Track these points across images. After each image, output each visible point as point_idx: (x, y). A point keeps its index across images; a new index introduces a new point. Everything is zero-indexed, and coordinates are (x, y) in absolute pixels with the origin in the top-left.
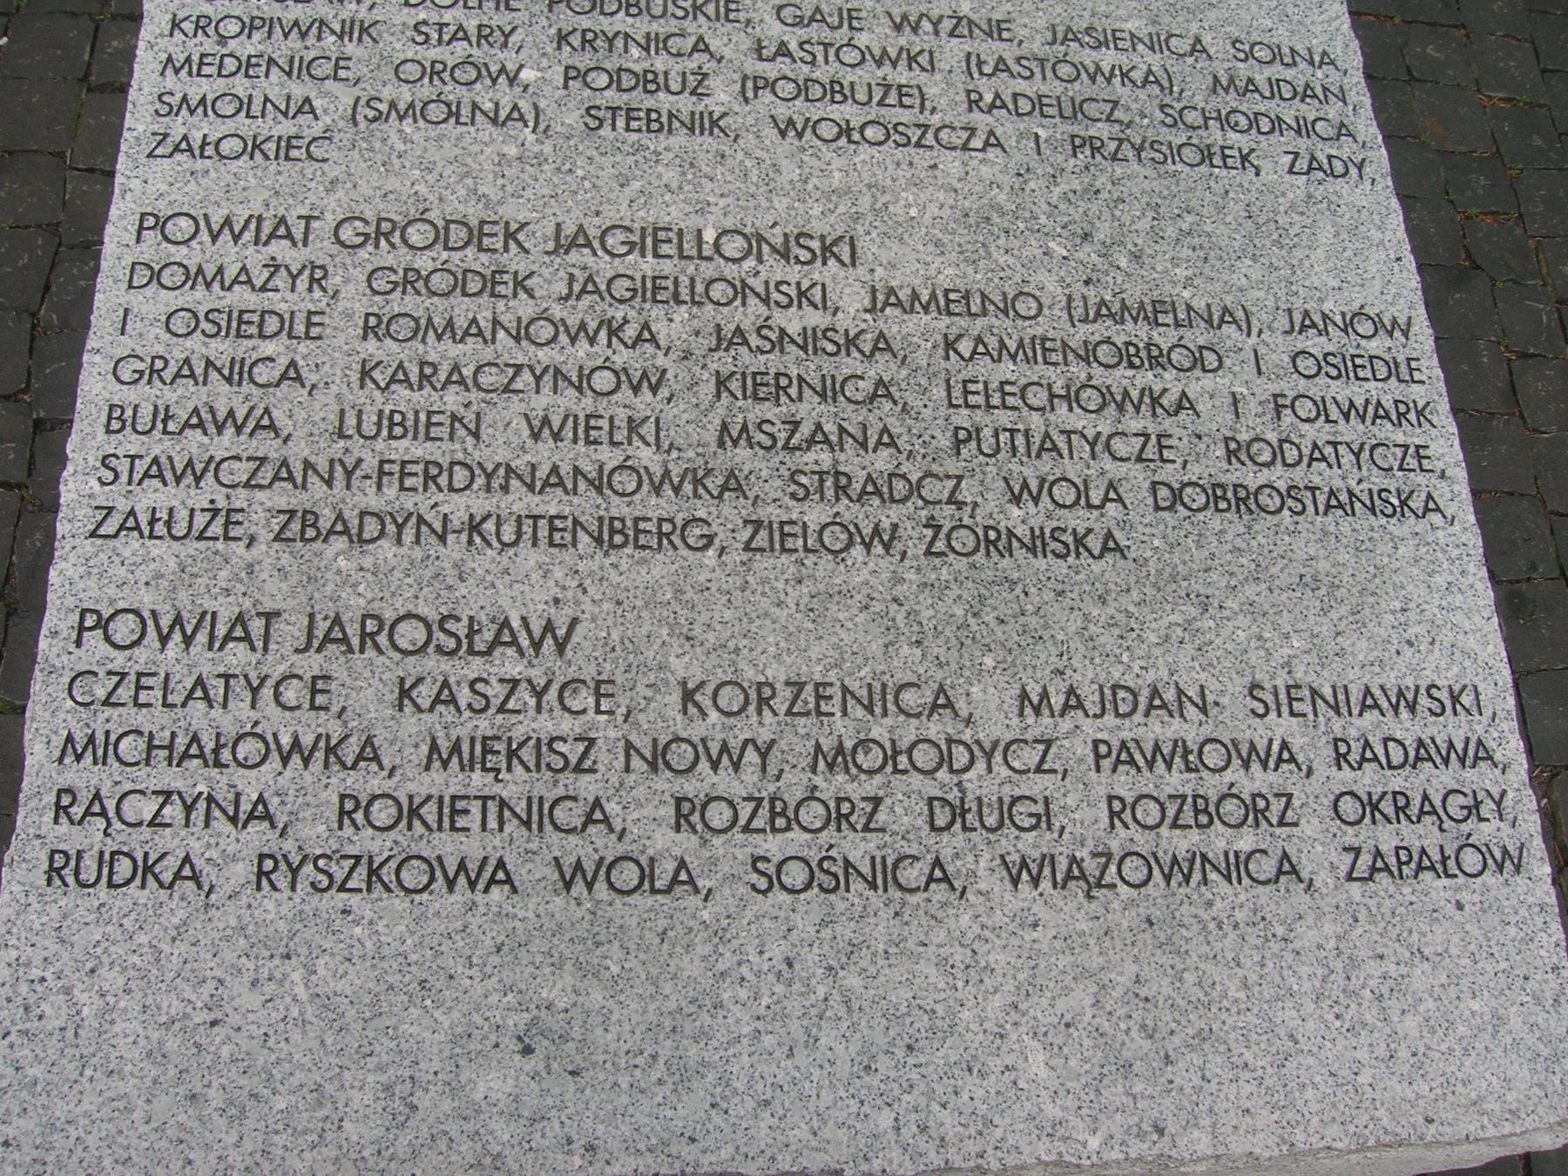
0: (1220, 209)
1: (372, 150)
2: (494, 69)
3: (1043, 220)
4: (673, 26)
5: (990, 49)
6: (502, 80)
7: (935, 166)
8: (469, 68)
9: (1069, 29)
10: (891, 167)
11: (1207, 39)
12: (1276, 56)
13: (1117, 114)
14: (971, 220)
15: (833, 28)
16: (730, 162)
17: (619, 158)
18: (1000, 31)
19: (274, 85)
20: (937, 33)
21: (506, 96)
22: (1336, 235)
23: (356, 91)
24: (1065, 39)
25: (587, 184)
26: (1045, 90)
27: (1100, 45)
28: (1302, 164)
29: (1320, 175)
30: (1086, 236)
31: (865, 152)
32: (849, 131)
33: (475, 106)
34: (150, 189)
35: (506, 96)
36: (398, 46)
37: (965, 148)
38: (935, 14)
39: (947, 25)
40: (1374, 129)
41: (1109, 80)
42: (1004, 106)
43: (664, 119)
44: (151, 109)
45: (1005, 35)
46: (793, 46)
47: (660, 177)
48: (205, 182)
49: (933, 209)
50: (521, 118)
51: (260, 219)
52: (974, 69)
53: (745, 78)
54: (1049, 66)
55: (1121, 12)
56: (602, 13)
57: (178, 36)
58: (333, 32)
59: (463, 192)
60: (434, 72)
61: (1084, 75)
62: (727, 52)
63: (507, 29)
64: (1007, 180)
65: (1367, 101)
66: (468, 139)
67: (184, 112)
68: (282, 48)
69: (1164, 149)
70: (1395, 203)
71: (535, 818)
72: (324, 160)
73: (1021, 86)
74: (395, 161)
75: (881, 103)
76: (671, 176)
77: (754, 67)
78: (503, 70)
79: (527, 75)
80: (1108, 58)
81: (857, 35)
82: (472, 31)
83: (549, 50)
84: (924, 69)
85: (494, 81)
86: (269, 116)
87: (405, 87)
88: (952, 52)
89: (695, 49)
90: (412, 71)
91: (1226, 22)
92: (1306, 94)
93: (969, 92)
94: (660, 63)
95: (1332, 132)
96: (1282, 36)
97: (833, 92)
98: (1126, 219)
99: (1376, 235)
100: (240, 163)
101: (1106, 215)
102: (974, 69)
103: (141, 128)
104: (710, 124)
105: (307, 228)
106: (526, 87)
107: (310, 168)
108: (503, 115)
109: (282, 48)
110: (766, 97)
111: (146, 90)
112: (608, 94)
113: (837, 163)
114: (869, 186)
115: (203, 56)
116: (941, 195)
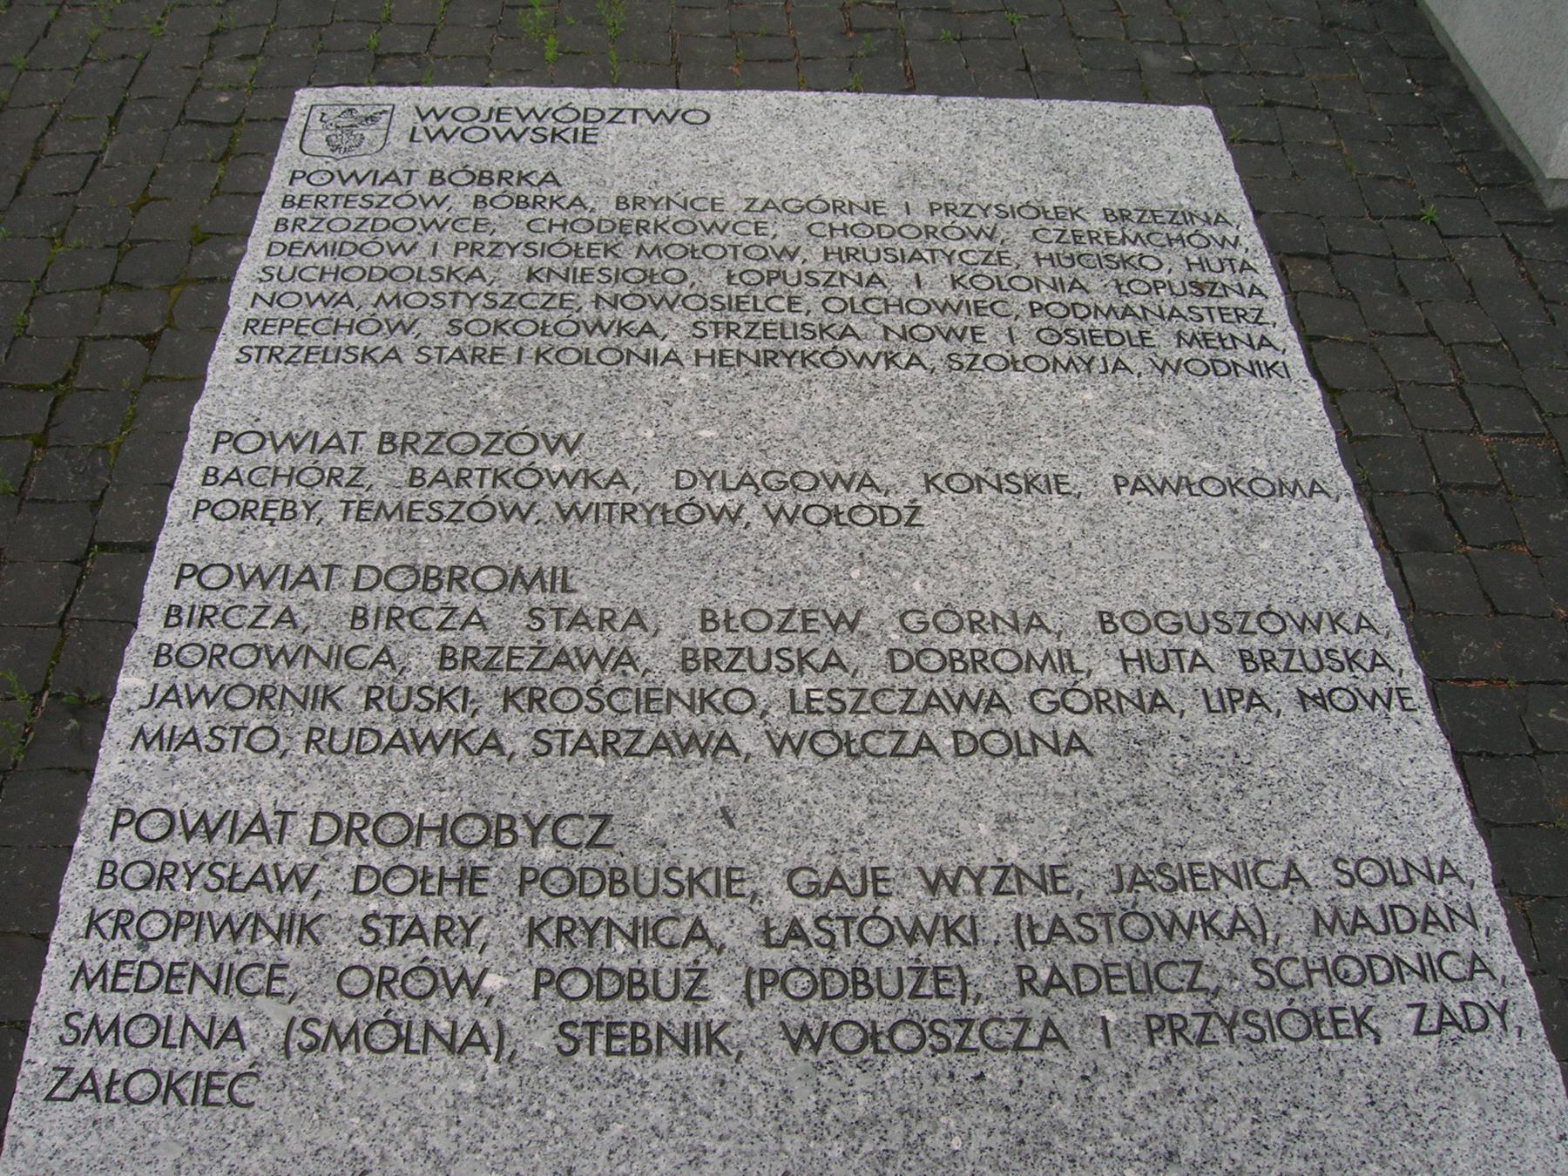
0: (1335, 1096)
1: (304, 1090)
2: (453, 975)
3: (1117, 1138)
4: (664, 906)
5: (1041, 906)
6: (462, 990)
7: (981, 1077)
8: (424, 975)
9: (1137, 869)
10: (928, 1082)
11: (1303, 863)
12: (1388, 874)
13: (1203, 980)
14: (1028, 1148)
15: (855, 896)
16: (731, 1090)
17: (597, 1092)
18: (1055, 879)
19: (198, 1003)
20: (979, 891)
21: (465, 1011)
22: (1482, 1114)
23: (292, 1010)
24: (1134, 882)
25: (558, 1131)
26: (1112, 956)
27: (1177, 885)
28: (1431, 1020)
29: (1454, 1031)
30: (1171, 1156)
31: (896, 1064)
32: (876, 1035)
33: (429, 1028)
34: (46, 1143)
35: (465, 1011)
36: (343, 948)
37: (1018, 1047)
38: (975, 865)
39: (991, 878)
40: (1514, 958)
41: (1188, 933)
42: (1063, 984)
43: (653, 1036)
44: (56, 1035)
45: (1061, 885)
46: (808, 924)
47: (646, 1116)
48: (109, 1134)
49: (980, 1138)
50: (483, 1043)
51: (282, 587)
52: (1026, 936)
53: (750, 973)
54: (1115, 921)
55: (1198, 838)
56: (582, 894)
57: (95, 937)
58: (270, 931)
59: (409, 1146)
60: (383, 982)
61: (1158, 931)
62: (729, 938)
63: (471, 920)
64: (1069, 1087)
65: (1501, 920)
66: (418, 1074)
67: (93, 1039)
68: (211, 952)
69: (1261, 1020)
70: (1549, 1058)
71: (692, 1042)
72: (249, 1105)
73: (1084, 953)
74: (332, 1105)
75: (914, 995)
76: (659, 1113)
77: (762, 956)
78: (463, 977)
79: (492, 982)
80: (1187, 903)
81: (884, 903)
82: (430, 925)
83: (518, 947)
84: (965, 943)
85: (452, 992)
86: (190, 1045)
87: (349, 1003)
88: (999, 912)
89: (691, 937)
90: (357, 980)
91: (1324, 836)
92: (1426, 921)
93: (1020, 968)
94: (649, 958)
95: (1463, 970)
96: (1392, 847)
97: (856, 983)
98: (1219, 1126)
99: (1531, 1107)
100: (150, 1108)
101: (1195, 1124)
102: (1026, 936)
103: (42, 1061)
104: (703, 1039)
105: (330, 575)
106: (490, 999)
107: (232, 1115)
108: (461, 1037)
109: (211, 952)
110: (776, 997)
111: (52, 1009)
112: (586, 1004)
113: (862, 1082)
114: (901, 1112)
115: (120, 963)
116: (990, 1117)
